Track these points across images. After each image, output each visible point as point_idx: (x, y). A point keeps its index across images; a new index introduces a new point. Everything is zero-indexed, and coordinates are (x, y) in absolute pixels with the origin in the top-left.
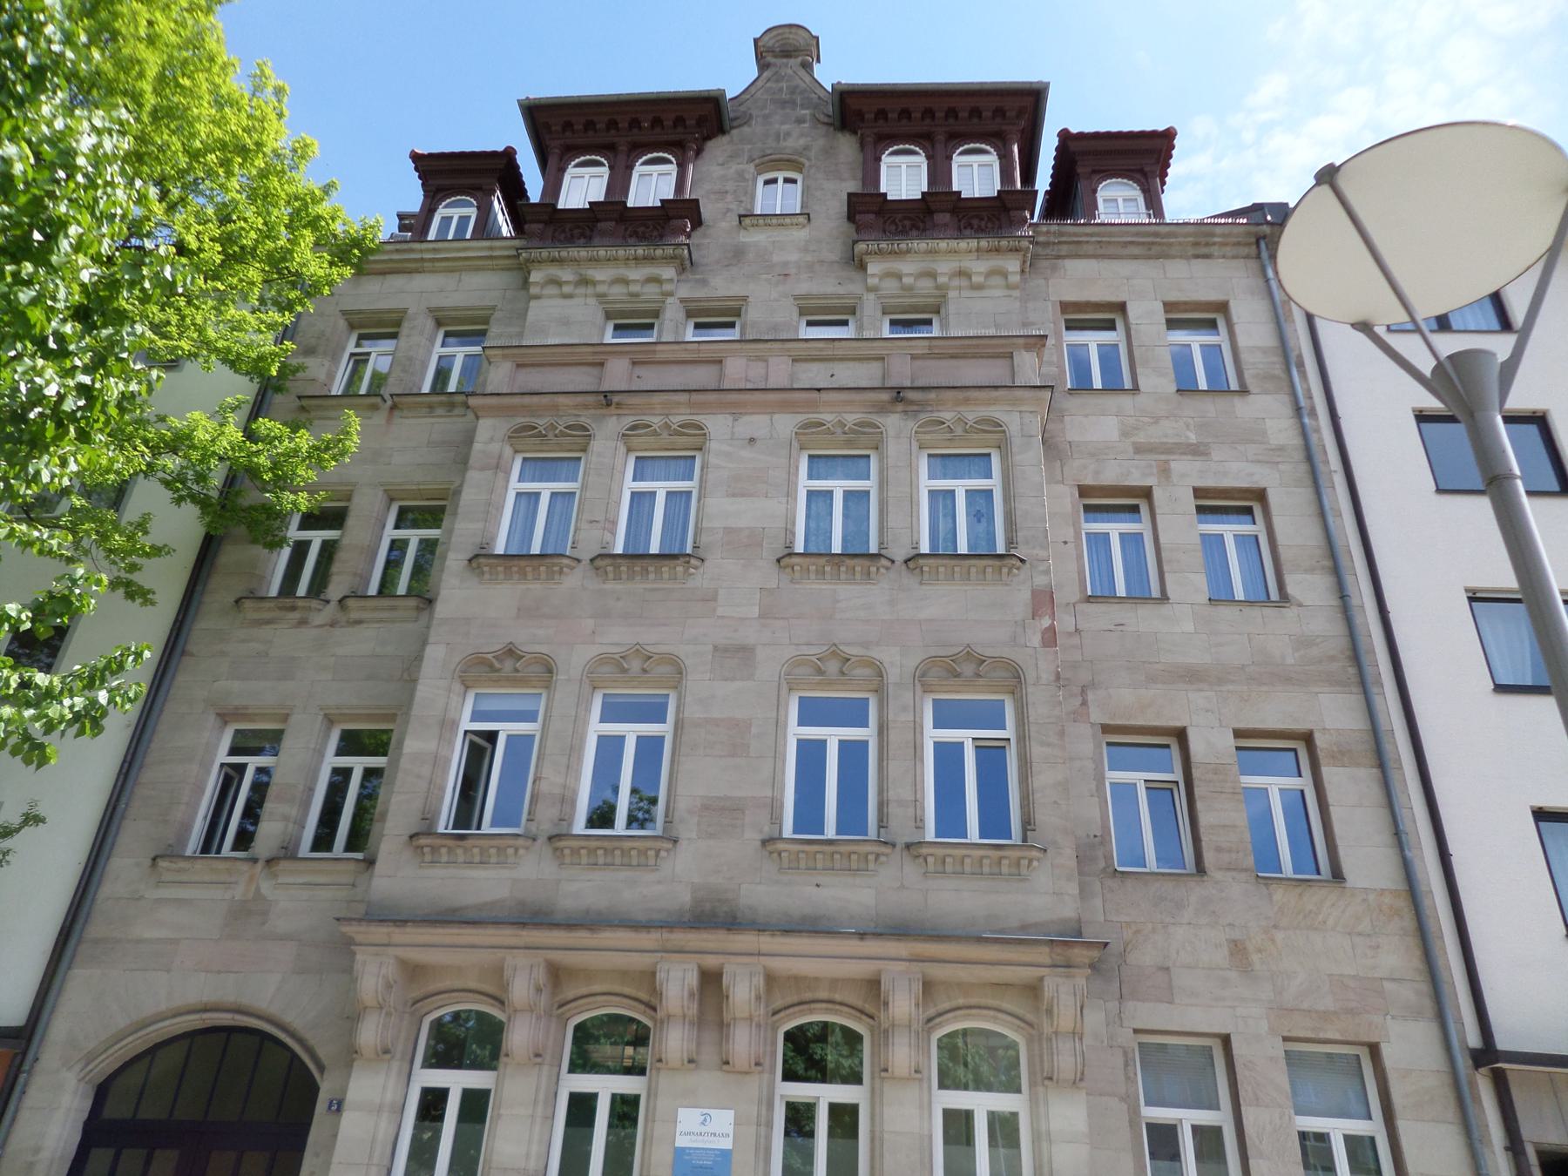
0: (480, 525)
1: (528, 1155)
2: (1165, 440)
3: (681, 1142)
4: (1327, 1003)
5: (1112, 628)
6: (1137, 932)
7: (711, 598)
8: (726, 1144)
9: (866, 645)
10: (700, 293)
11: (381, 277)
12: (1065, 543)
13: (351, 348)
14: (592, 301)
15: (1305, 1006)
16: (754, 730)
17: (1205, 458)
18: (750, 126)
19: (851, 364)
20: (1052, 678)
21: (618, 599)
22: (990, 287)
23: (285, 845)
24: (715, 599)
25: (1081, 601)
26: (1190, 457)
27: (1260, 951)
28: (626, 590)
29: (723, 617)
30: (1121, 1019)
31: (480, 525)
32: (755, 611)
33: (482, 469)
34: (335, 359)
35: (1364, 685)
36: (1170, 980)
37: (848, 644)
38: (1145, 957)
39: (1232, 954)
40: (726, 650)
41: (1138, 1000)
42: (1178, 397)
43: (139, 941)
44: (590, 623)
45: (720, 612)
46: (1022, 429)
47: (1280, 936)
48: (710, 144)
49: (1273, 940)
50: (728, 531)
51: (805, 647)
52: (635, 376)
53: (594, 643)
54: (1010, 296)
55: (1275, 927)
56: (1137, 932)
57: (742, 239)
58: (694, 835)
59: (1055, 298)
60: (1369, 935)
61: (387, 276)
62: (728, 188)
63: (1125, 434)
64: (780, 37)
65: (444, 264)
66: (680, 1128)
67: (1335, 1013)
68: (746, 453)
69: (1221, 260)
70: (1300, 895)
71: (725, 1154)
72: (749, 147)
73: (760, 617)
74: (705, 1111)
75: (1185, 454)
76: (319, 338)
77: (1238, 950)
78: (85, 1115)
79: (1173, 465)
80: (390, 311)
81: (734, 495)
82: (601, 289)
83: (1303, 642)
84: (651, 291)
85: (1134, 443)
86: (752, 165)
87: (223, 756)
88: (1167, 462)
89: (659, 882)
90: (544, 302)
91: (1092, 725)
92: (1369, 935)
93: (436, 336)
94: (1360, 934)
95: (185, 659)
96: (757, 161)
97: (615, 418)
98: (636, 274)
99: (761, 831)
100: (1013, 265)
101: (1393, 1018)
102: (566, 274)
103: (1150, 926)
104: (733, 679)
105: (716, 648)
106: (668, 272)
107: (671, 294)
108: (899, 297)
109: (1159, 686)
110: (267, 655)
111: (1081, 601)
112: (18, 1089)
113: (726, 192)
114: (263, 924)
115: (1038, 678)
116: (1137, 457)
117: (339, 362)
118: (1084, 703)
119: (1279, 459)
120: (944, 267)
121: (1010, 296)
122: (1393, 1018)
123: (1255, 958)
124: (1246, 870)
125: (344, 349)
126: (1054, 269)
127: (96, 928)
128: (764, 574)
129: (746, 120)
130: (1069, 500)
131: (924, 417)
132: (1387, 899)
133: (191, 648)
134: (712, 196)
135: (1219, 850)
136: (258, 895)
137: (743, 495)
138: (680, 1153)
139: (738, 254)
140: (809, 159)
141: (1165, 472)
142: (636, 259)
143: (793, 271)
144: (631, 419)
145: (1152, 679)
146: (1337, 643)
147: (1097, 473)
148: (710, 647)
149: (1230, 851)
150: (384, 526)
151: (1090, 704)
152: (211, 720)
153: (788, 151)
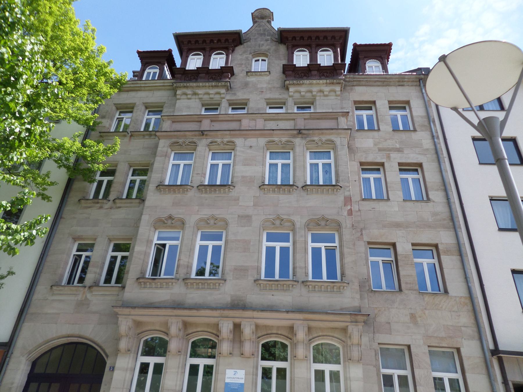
0: (160, 175)
1: (176, 385)
2: (388, 147)
3: (227, 381)
4: (443, 334)
5: (371, 209)
6: (379, 311)
7: (237, 199)
8: (242, 381)
9: (289, 215)
10: (234, 98)
11: (127, 92)
12: (355, 181)
13: (117, 116)
14: (197, 100)
15: (435, 335)
16: (251, 243)
17: (402, 153)
18: (250, 42)
19: (284, 121)
20: (351, 226)
21: (206, 200)
22: (330, 96)
23: (95, 282)
24: (238, 200)
25: (361, 200)
26: (397, 152)
27: (420, 317)
28: (209, 197)
29: (241, 206)
30: (374, 340)
31: (160, 175)
32: (252, 204)
33: (161, 156)
34: (112, 120)
35: (455, 228)
36: (390, 327)
37: (283, 215)
38: (382, 319)
39: (411, 318)
40: (242, 217)
41: (380, 333)
42: (393, 132)
43: (46, 314)
44: (197, 208)
45: (240, 204)
46: (341, 143)
47: (427, 312)
48: (237, 48)
49: (425, 313)
50: (243, 177)
51: (268, 216)
52: (212, 125)
53: (198, 214)
54: (337, 99)
55: (425, 309)
56: (379, 311)
57: (248, 80)
58: (231, 278)
59: (352, 99)
60: (457, 312)
61: (129, 92)
62: (243, 63)
63: (375, 145)
64: (260, 12)
65: (148, 88)
66: (227, 376)
67: (445, 338)
68: (249, 151)
69: (407, 87)
70: (434, 298)
71: (242, 385)
72: (250, 49)
73: (254, 206)
74: (235, 370)
75: (395, 151)
76: (106, 113)
77: (413, 317)
78: (28, 372)
79: (391, 155)
80: (130, 104)
81: (245, 165)
82: (200, 96)
83: (435, 214)
84: (217, 97)
85: (378, 148)
86: (251, 55)
87: (74, 252)
88: (389, 154)
89: (220, 294)
90: (181, 101)
91: (364, 242)
92: (457, 312)
93: (145, 112)
94: (454, 311)
95: (62, 220)
96: (253, 54)
97: (205, 139)
98: (212, 91)
99: (254, 277)
100: (338, 88)
101: (465, 339)
102: (189, 91)
103: (384, 309)
104: (245, 226)
105: (239, 216)
106: (223, 91)
107: (224, 98)
108: (300, 99)
109: (387, 229)
110: (89, 218)
111: (361, 200)
112: (6, 363)
113: (242, 64)
114: (88, 308)
115: (346, 226)
116: (379, 152)
117: (113, 121)
118: (362, 234)
119: (427, 153)
120: (315, 89)
121: (337, 99)
122: (465, 339)
123: (419, 319)
124: (416, 290)
125: (115, 116)
126: (352, 90)
127: (32, 309)
128: (255, 191)
129: (249, 40)
130: (356, 167)
131: (308, 139)
132: (463, 300)
133: (64, 216)
134: (238, 65)
135: (406, 283)
136: (86, 298)
137: (248, 165)
138: (227, 384)
139: (246, 85)
140: (270, 53)
141: (389, 157)
142: (212, 86)
143: (264, 90)
144: (211, 140)
145: (384, 226)
146: (446, 214)
147: (366, 158)
148: (237, 216)
149: (410, 284)
150: (128, 175)
151: (363, 235)
152: (71, 240)
153: (263, 50)
